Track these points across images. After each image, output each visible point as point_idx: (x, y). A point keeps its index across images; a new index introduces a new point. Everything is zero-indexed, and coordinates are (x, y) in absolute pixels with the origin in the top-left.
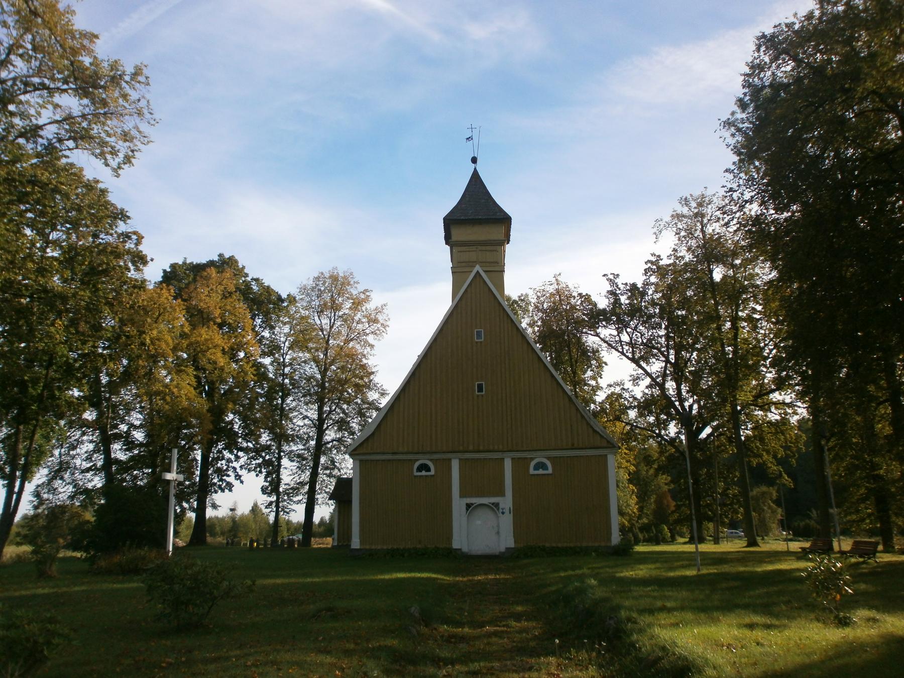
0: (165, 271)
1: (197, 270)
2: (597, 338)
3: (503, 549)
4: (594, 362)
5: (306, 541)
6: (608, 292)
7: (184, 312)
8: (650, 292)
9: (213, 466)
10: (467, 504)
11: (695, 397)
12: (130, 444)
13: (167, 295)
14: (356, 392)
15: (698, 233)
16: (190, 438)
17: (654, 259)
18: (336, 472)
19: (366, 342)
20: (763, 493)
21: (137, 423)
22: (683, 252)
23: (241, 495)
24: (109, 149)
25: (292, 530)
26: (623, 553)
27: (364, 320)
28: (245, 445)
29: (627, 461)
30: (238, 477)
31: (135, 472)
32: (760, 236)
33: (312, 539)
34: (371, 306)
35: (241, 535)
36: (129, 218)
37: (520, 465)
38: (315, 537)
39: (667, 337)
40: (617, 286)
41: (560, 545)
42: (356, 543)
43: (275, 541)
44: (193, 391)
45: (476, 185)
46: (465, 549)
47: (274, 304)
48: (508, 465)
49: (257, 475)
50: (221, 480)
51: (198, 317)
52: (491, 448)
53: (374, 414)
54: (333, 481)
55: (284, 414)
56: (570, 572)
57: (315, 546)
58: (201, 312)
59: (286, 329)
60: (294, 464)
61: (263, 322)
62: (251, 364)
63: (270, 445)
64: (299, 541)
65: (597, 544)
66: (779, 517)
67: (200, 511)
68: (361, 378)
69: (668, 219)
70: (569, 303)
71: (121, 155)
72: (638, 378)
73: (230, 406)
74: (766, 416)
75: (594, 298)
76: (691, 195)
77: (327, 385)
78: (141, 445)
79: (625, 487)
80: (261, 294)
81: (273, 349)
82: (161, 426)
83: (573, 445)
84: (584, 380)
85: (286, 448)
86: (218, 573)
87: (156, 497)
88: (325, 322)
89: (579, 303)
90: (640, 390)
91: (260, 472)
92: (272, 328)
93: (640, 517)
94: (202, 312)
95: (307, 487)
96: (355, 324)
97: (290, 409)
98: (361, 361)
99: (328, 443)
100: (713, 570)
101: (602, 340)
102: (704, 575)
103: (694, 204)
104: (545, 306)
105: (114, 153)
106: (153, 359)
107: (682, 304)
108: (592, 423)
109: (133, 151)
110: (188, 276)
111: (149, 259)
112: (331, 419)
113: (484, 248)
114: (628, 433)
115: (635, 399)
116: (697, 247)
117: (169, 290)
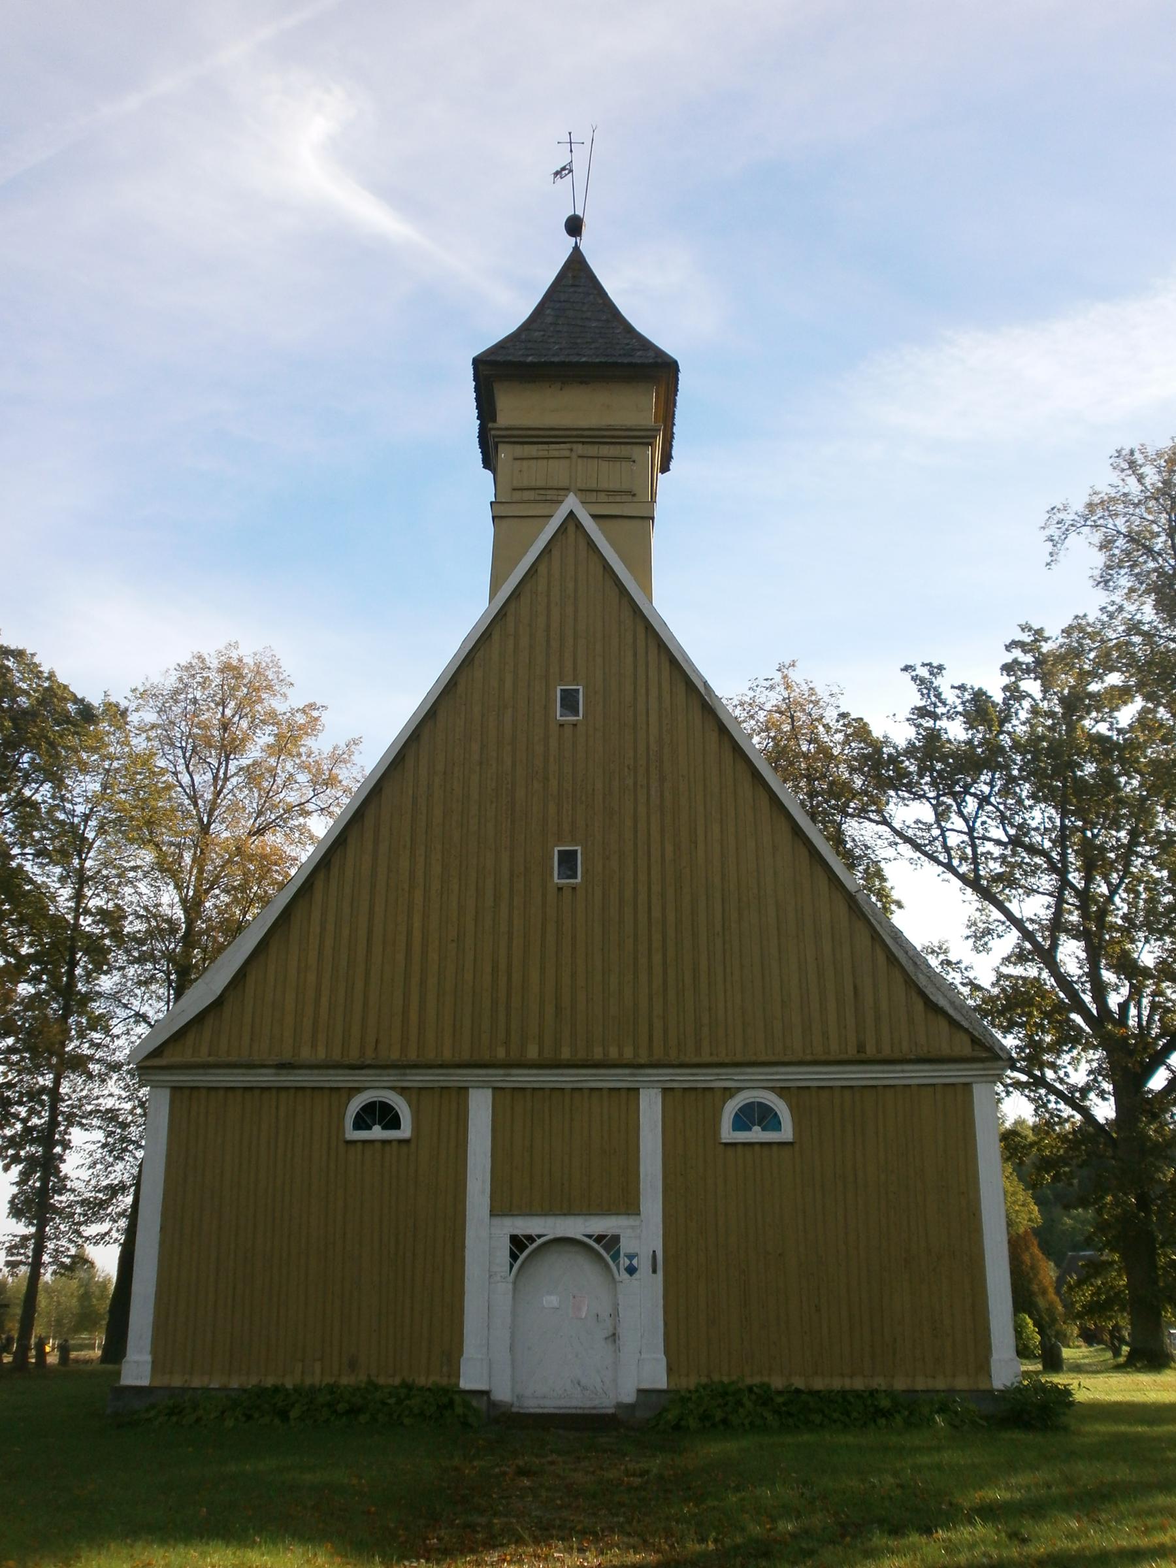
2: (883, 829)
3: (628, 1396)
10: (514, 1239)
17: (1027, 638)
37: (690, 1110)
40: (938, 696)
41: (819, 1384)
46: (503, 1393)
48: (651, 1109)
65: (941, 1384)
72: (988, 932)
83: (861, 1048)
113: (592, 450)
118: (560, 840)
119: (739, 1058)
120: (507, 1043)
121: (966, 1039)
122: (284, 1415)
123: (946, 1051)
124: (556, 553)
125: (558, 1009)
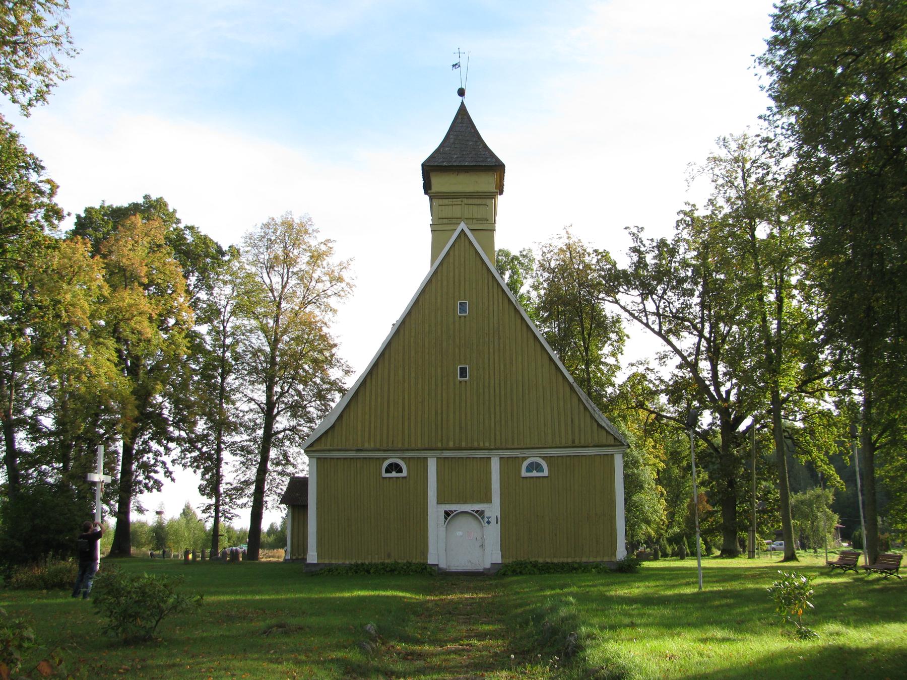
0: (78, 217)
1: (118, 215)
3: (488, 566)
4: (613, 336)
5: (252, 553)
6: (630, 248)
7: (104, 272)
8: (682, 250)
9: (138, 460)
11: (734, 381)
12: (35, 431)
13: (83, 249)
14: (314, 369)
15: (739, 182)
16: (111, 425)
17: (688, 209)
18: (290, 469)
19: (327, 306)
20: (818, 496)
21: (45, 406)
22: (721, 202)
23: (172, 496)
24: (19, 83)
25: (234, 539)
26: (627, 570)
27: (324, 278)
28: (176, 433)
29: (656, 457)
30: (168, 473)
31: (44, 467)
32: (798, 196)
33: (260, 551)
34: (332, 261)
35: (172, 545)
36: (43, 168)
38: (263, 547)
39: (702, 305)
40: (641, 242)
41: (555, 561)
42: (312, 557)
43: (214, 553)
44: (115, 369)
45: (463, 123)
46: (443, 565)
47: (213, 258)
48: (495, 466)
49: (195, 472)
50: (148, 477)
51: (120, 277)
52: (476, 444)
53: (337, 396)
54: (287, 480)
55: (224, 395)
56: (558, 591)
57: (264, 560)
58: (123, 270)
59: (228, 290)
60: (238, 458)
61: (199, 280)
62: (183, 335)
63: (207, 435)
64: (244, 553)
65: (598, 559)
66: (836, 524)
67: (122, 515)
68: (321, 352)
69: (704, 162)
70: (581, 262)
71: (33, 91)
72: (666, 356)
73: (159, 387)
74: (818, 404)
75: (613, 256)
76: (731, 135)
77: (278, 359)
78: (51, 433)
79: (651, 489)
80: (197, 246)
81: (212, 314)
82: (76, 411)
83: (573, 442)
84: (598, 357)
85: (227, 439)
86: (165, 586)
87: (75, 497)
88: (276, 280)
89: (594, 261)
90: (669, 371)
91: (198, 467)
92: (210, 288)
93: (670, 526)
94: (125, 270)
95: (253, 487)
96: (313, 283)
97: (232, 390)
98: (320, 329)
99: (279, 432)
100: (717, 588)
101: (622, 307)
102: (705, 593)
103: (733, 146)
104: (553, 264)
105: (25, 87)
106: (67, 327)
107: (717, 268)
108: (596, 416)
109: (47, 86)
110: (107, 223)
111: (65, 213)
112: (283, 402)
113: (470, 201)
114: (652, 424)
115: (662, 381)
116: (737, 198)
117: (85, 244)
118: (460, 363)
119: (528, 446)
120: (441, 441)
121: (612, 438)
122: (368, 572)
123: (604, 442)
124: (457, 246)
125: (460, 427)
